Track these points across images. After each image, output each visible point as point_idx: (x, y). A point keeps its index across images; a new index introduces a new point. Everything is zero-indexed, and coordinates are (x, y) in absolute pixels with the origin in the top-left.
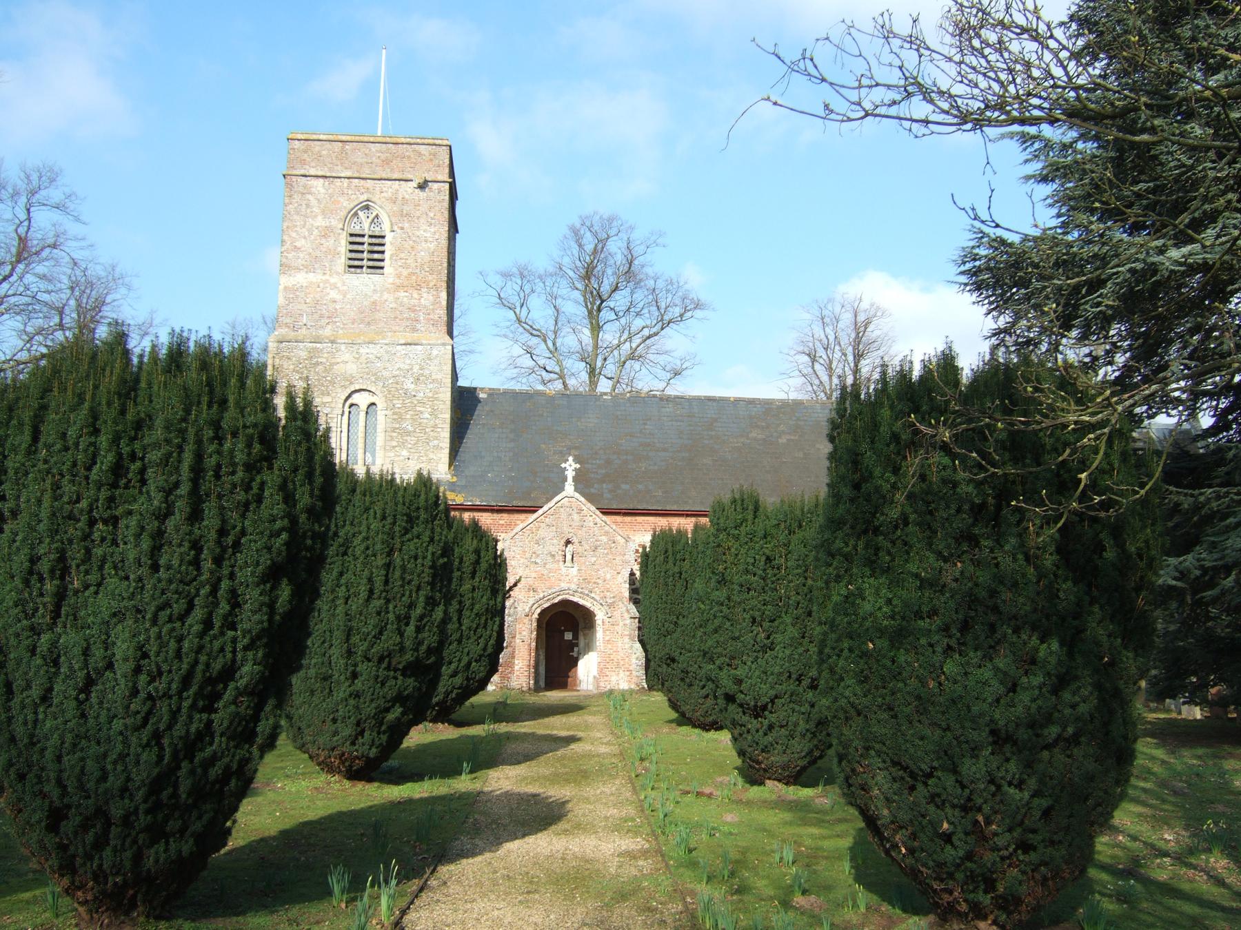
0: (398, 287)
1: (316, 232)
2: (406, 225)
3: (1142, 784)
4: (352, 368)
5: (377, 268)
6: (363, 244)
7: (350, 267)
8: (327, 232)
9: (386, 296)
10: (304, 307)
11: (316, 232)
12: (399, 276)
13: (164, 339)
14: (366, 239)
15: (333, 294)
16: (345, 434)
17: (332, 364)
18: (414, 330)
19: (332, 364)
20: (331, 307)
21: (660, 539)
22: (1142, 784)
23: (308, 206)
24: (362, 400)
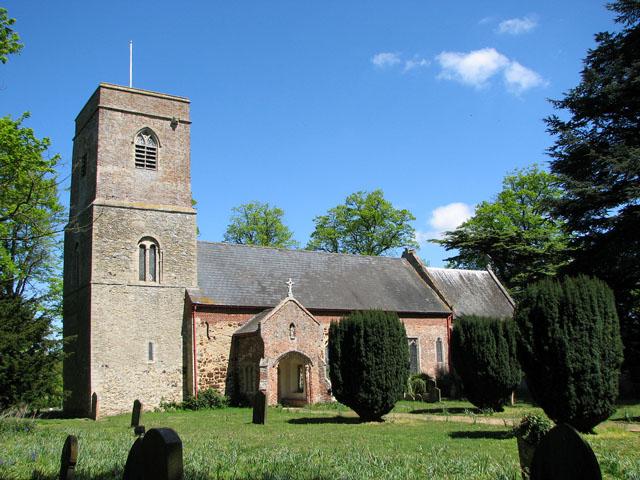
0: (165, 179)
1: (118, 142)
2: (168, 144)
3: (15, 286)
4: (142, 224)
5: (152, 166)
6: (143, 157)
7: (137, 165)
8: (124, 143)
9: (158, 183)
10: (111, 185)
11: (118, 142)
12: (165, 172)
13: (39, 137)
14: (145, 150)
15: (129, 179)
16: (157, 261)
17: (131, 221)
18: (174, 204)
19: (131, 221)
20: (128, 187)
21: (333, 326)
22: (15, 286)
23: (113, 126)
24: (148, 244)
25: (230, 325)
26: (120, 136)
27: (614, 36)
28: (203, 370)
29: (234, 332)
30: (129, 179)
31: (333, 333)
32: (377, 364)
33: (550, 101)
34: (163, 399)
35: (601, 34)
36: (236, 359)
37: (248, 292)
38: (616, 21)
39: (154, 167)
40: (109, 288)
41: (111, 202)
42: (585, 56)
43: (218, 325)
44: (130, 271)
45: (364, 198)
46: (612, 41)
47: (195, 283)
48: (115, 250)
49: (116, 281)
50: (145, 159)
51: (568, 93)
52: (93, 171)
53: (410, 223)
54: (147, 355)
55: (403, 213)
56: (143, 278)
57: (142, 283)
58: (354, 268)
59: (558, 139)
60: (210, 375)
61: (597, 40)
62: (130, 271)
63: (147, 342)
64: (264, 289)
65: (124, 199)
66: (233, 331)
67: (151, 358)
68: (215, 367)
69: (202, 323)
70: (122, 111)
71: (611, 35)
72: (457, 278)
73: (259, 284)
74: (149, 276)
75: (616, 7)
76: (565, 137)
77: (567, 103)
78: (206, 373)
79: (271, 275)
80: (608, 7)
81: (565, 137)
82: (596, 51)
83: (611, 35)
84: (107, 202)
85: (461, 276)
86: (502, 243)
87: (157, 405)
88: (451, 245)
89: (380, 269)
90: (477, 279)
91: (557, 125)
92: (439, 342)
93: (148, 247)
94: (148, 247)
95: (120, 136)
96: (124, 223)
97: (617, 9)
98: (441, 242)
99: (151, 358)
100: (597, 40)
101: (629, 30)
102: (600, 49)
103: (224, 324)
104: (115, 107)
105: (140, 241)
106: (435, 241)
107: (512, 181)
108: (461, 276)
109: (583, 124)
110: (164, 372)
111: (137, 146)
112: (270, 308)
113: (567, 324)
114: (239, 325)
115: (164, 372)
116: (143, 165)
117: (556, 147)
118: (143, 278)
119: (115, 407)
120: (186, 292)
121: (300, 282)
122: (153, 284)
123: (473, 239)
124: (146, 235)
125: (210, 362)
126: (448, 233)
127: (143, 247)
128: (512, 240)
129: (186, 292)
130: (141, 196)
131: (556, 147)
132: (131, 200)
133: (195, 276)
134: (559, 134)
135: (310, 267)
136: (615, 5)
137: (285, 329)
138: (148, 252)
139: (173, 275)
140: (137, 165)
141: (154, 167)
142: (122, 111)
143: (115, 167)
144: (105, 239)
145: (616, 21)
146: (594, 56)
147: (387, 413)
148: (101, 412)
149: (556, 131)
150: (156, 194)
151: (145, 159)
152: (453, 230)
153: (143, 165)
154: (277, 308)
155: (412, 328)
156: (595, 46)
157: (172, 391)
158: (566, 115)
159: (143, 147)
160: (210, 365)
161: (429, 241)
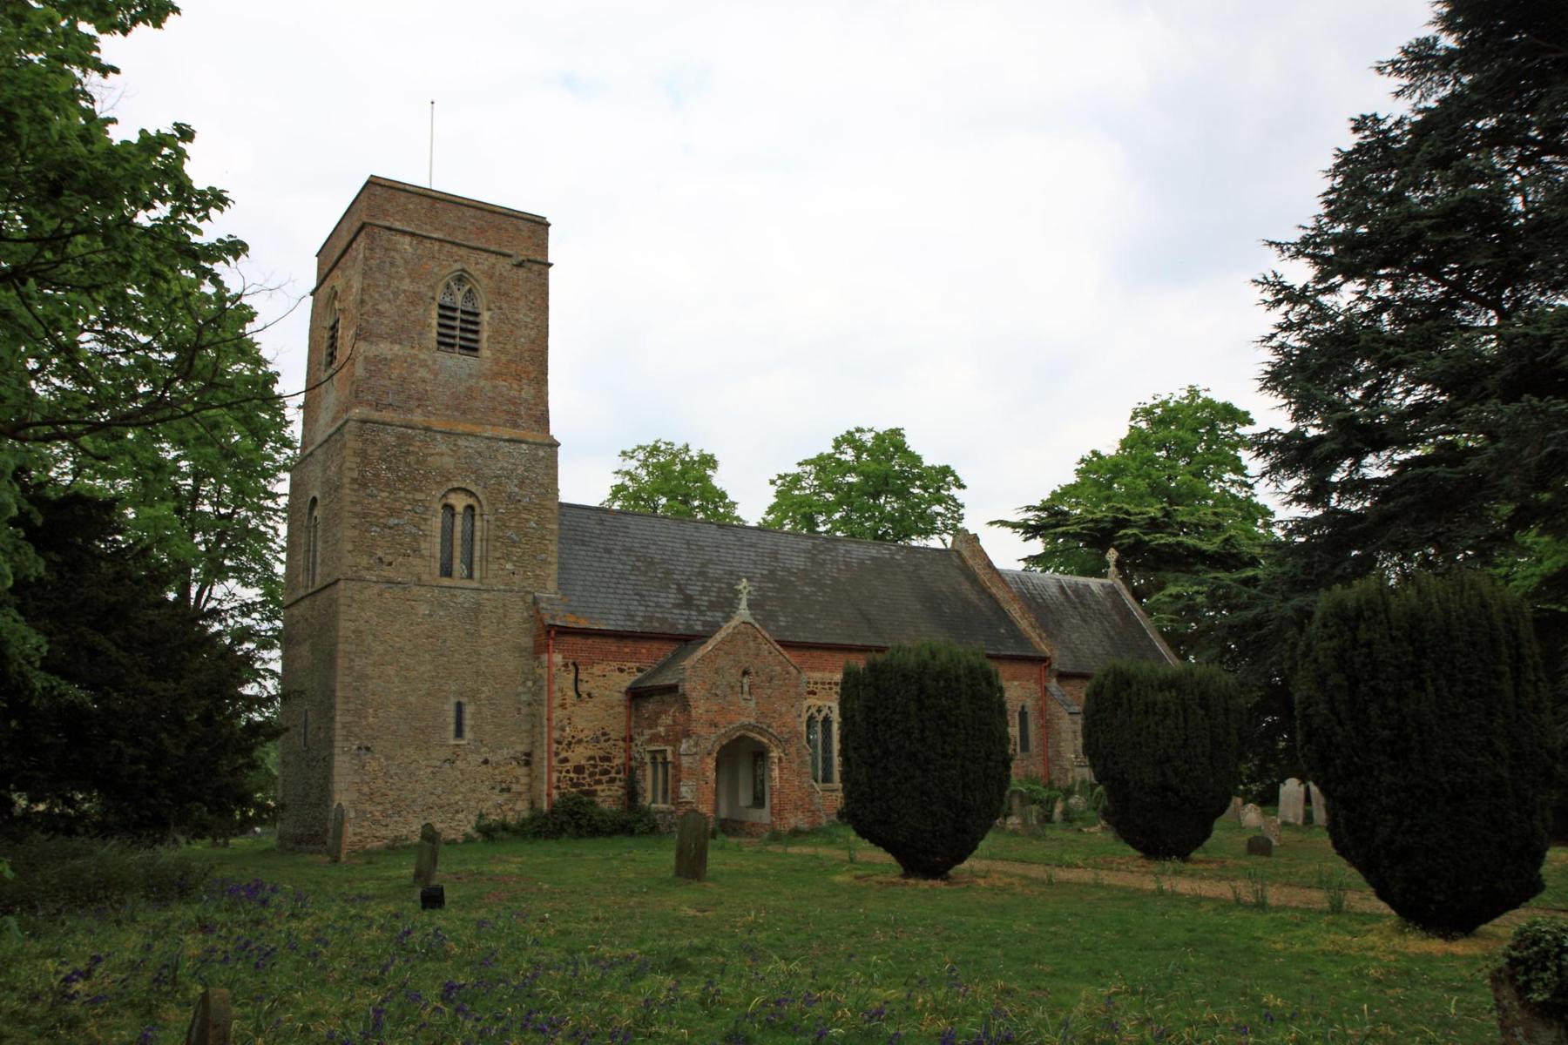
2: (505, 306)
4: (448, 462)
5: (471, 349)
8: (415, 299)
9: (482, 383)
10: (387, 382)
14: (458, 314)
15: (423, 373)
18: (515, 425)
20: (421, 386)
23: (392, 264)
24: (460, 502)
25: (621, 671)
26: (406, 285)
27: (1390, 122)
28: (566, 760)
29: (628, 684)
30: (423, 373)
31: (850, 687)
32: (944, 756)
33: (1271, 243)
34: (481, 816)
35: (1364, 117)
36: (632, 739)
37: (658, 605)
38: (1397, 94)
39: (476, 350)
40: (376, 589)
41: (387, 415)
42: (1330, 162)
43: (597, 670)
44: (422, 557)
45: (868, 438)
46: (1384, 132)
47: (552, 585)
48: (393, 512)
49: (389, 573)
50: (457, 332)
51: (1311, 223)
52: (363, 204)
53: (954, 491)
54: (452, 727)
55: (946, 471)
56: (447, 571)
57: (446, 581)
58: (861, 563)
59: (1281, 320)
60: (579, 769)
61: (1355, 130)
62: (422, 557)
63: (453, 700)
64: (688, 602)
65: (410, 411)
66: (627, 681)
67: (459, 732)
68: (590, 753)
69: (566, 665)
70: (413, 235)
71: (1384, 120)
72: (1054, 590)
73: (680, 590)
74: (458, 567)
75: (1396, 67)
76: (1293, 317)
77: (1305, 247)
78: (569, 766)
79: (702, 574)
80: (1380, 70)
81: (1293, 317)
82: (1350, 153)
83: (1384, 120)
84: (376, 415)
85: (1062, 588)
86: (1135, 531)
87: (469, 829)
88: (1031, 531)
89: (911, 568)
90: (1092, 593)
91: (1285, 294)
92: (827, 722)
93: (460, 508)
94: (460, 508)
95: (406, 285)
96: (411, 459)
97: (1399, 71)
98: (1014, 526)
99: (459, 732)
100: (1355, 130)
101: (1426, 109)
102: (1360, 148)
103: (609, 667)
104: (398, 225)
105: (444, 496)
106: (1004, 523)
107: (1148, 412)
108: (1062, 588)
109: (1332, 289)
110: (486, 762)
111: (441, 307)
112: (702, 638)
113: (1434, 680)
114: (639, 670)
115: (486, 762)
116: (452, 346)
117: (1273, 336)
118: (447, 571)
119: (383, 832)
120: (535, 602)
121: (760, 588)
122: (467, 583)
123: (1080, 520)
124: (456, 485)
125: (580, 741)
126: (1028, 509)
127: (449, 508)
128: (1154, 525)
129: (535, 602)
130: (448, 407)
131: (1273, 336)
132: (427, 414)
133: (553, 570)
134: (1285, 307)
135: (777, 560)
136: (1394, 63)
137: (733, 680)
138: (459, 520)
139: (509, 566)
140: (440, 343)
141: (476, 350)
142: (413, 235)
143: (396, 347)
144: (371, 490)
145: (1397, 94)
146: (1346, 162)
147: (961, 859)
148: (352, 844)
149: (1279, 302)
150: (478, 404)
151: (457, 323)
152: (1038, 503)
153: (452, 346)
154: (719, 637)
155: (1017, 691)
156: (1350, 141)
157: (500, 800)
158: (1300, 273)
159: (454, 310)
160: (580, 749)
161: (992, 523)
